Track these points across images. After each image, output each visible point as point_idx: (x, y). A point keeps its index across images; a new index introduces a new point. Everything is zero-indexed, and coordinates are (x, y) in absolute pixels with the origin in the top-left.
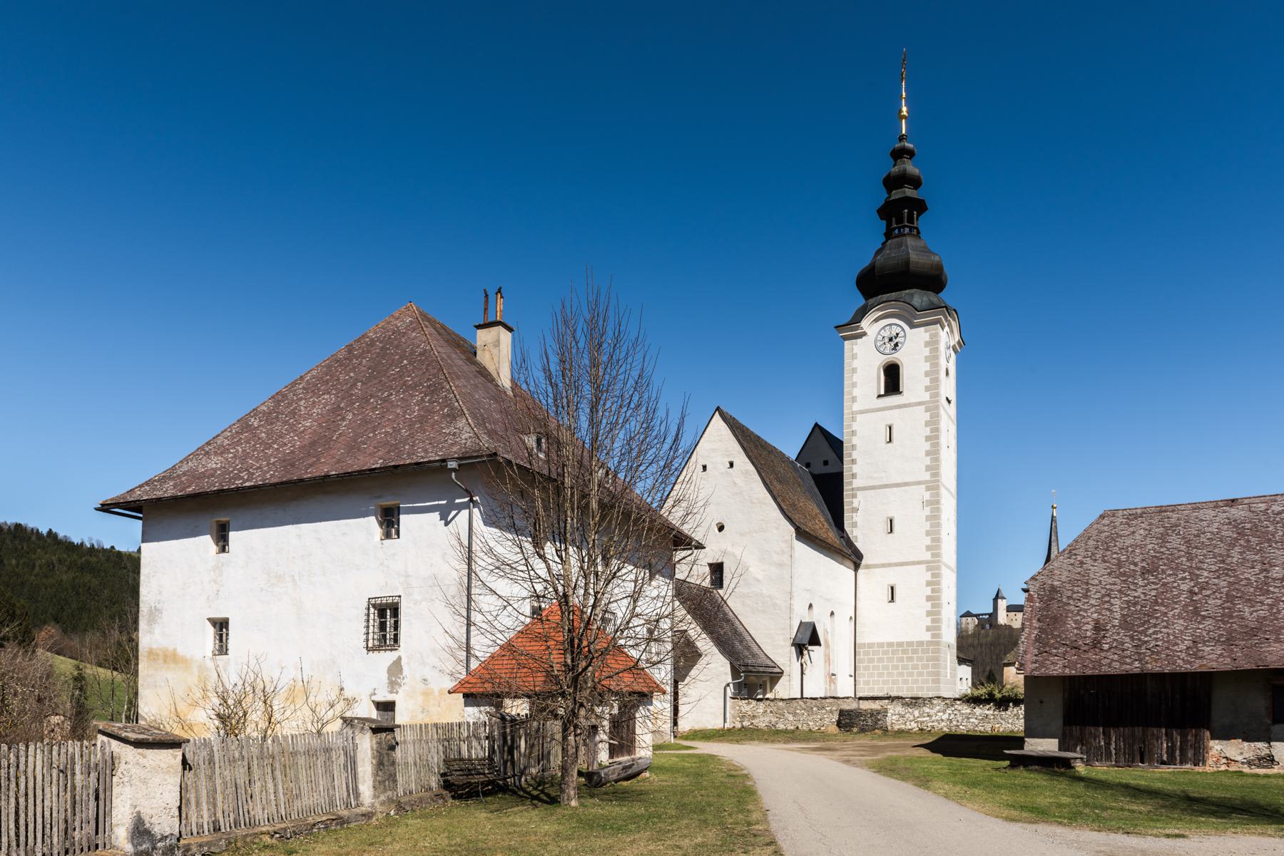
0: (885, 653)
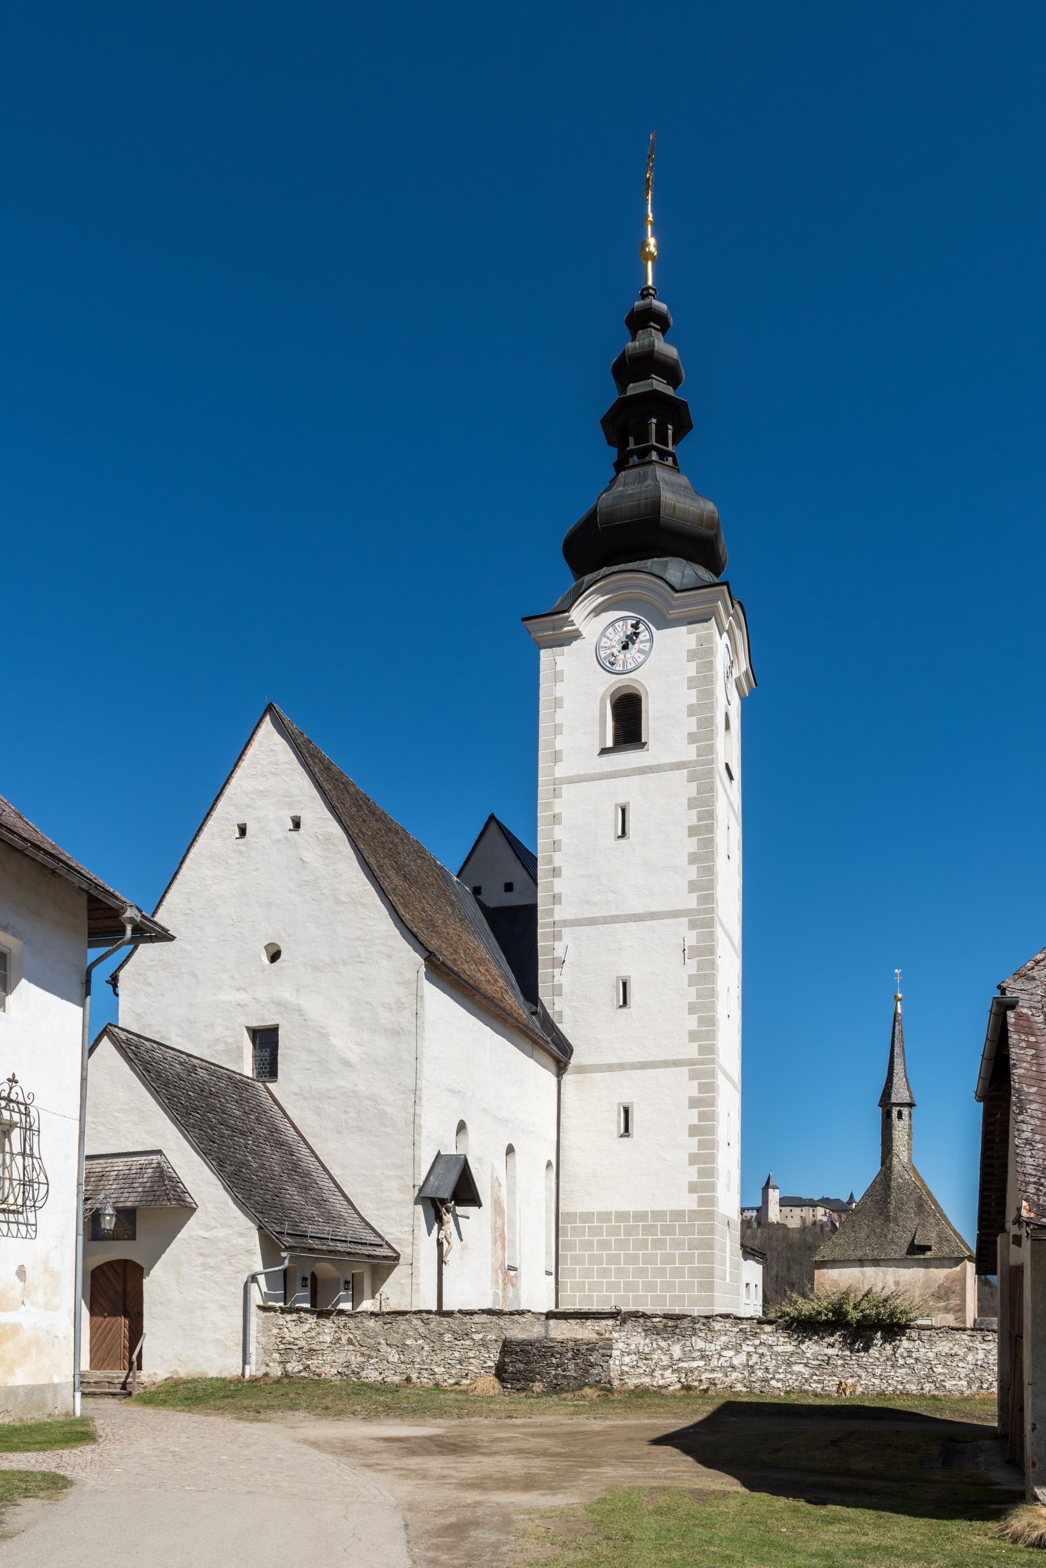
0: (612, 1231)
